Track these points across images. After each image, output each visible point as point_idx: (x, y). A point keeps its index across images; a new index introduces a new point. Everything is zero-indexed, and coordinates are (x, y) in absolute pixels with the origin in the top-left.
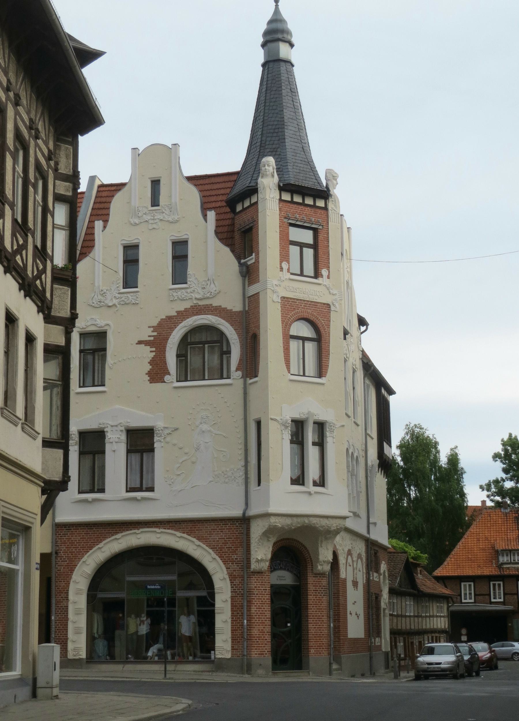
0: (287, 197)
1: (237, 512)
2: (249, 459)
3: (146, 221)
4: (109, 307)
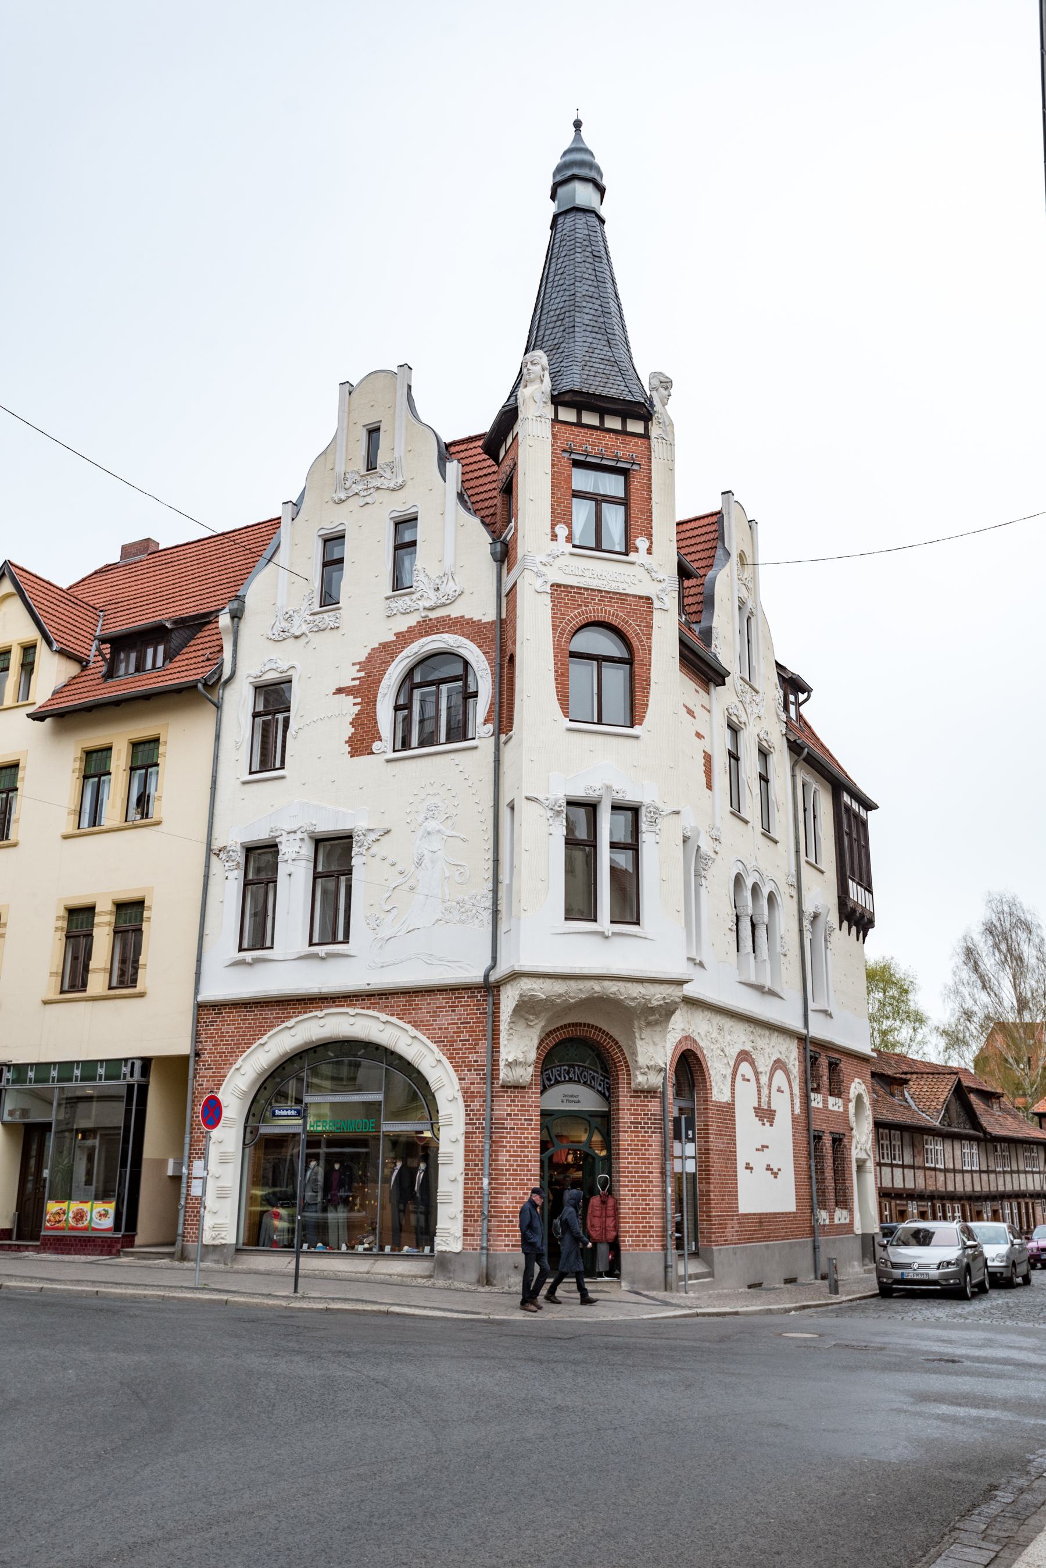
0: (568, 415)
1: (474, 974)
2: (501, 877)
3: (357, 494)
4: (297, 637)
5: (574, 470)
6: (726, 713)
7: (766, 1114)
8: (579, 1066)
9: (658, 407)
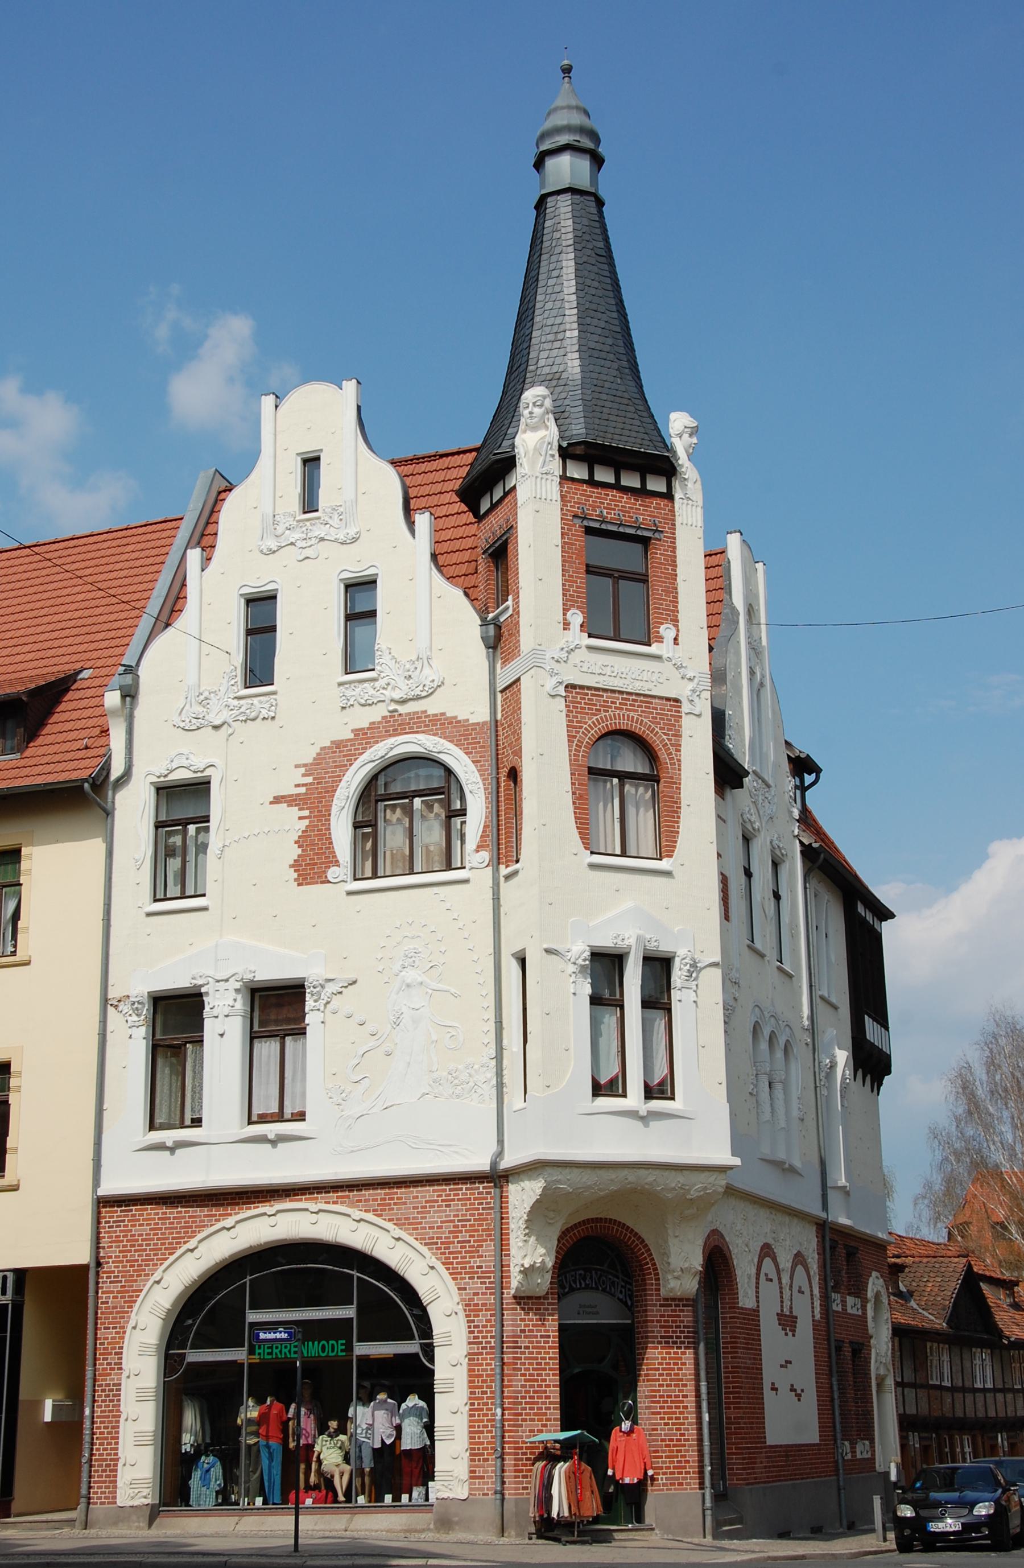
0: (578, 471)
1: (481, 1163)
2: (505, 1042)
3: (292, 544)
4: (216, 728)
8: (596, 1270)
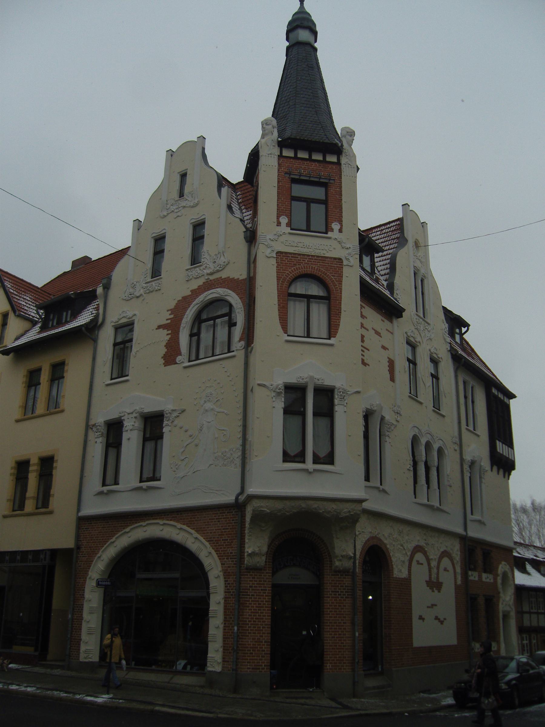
1: (230, 498)
3: (173, 211)
4: (138, 297)
5: (293, 186)
6: (405, 335)
7: (435, 585)
9: (345, 145)
